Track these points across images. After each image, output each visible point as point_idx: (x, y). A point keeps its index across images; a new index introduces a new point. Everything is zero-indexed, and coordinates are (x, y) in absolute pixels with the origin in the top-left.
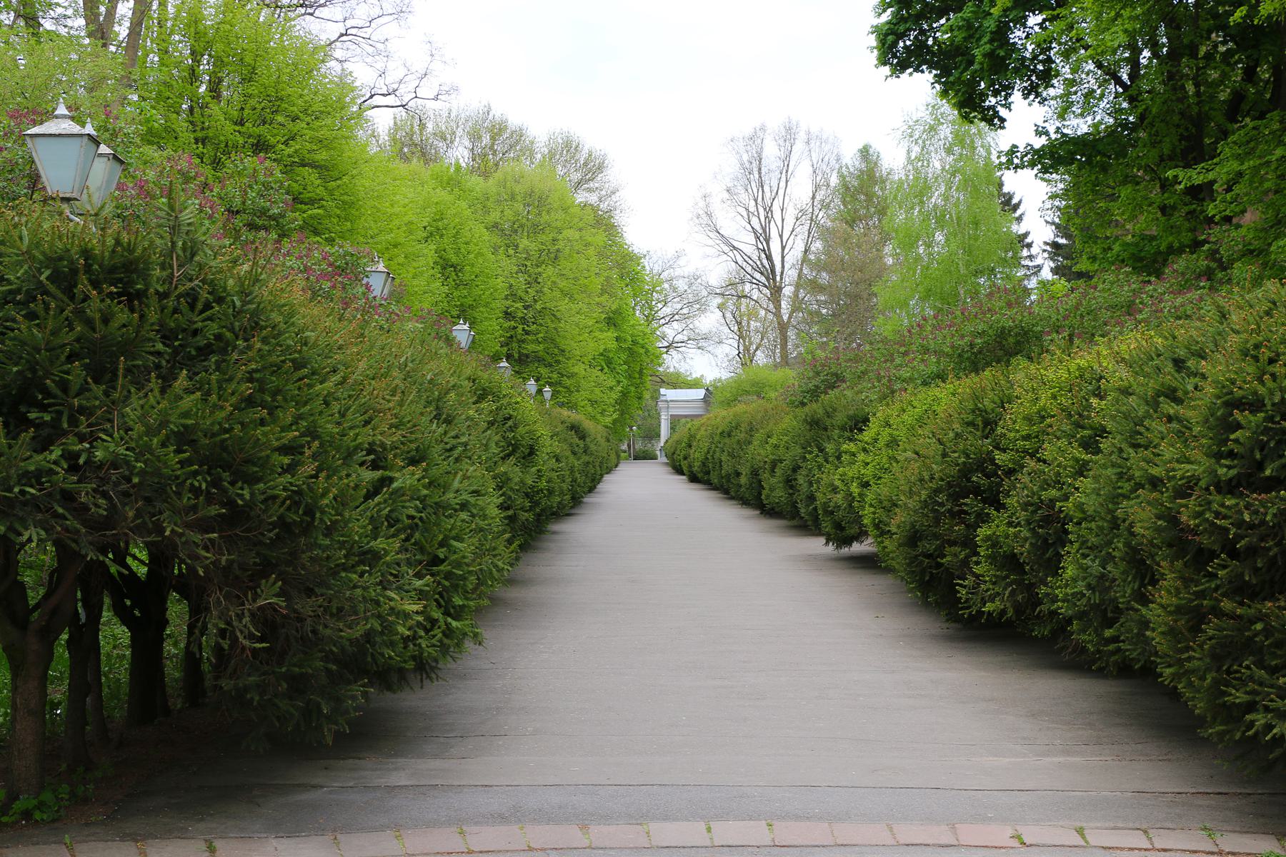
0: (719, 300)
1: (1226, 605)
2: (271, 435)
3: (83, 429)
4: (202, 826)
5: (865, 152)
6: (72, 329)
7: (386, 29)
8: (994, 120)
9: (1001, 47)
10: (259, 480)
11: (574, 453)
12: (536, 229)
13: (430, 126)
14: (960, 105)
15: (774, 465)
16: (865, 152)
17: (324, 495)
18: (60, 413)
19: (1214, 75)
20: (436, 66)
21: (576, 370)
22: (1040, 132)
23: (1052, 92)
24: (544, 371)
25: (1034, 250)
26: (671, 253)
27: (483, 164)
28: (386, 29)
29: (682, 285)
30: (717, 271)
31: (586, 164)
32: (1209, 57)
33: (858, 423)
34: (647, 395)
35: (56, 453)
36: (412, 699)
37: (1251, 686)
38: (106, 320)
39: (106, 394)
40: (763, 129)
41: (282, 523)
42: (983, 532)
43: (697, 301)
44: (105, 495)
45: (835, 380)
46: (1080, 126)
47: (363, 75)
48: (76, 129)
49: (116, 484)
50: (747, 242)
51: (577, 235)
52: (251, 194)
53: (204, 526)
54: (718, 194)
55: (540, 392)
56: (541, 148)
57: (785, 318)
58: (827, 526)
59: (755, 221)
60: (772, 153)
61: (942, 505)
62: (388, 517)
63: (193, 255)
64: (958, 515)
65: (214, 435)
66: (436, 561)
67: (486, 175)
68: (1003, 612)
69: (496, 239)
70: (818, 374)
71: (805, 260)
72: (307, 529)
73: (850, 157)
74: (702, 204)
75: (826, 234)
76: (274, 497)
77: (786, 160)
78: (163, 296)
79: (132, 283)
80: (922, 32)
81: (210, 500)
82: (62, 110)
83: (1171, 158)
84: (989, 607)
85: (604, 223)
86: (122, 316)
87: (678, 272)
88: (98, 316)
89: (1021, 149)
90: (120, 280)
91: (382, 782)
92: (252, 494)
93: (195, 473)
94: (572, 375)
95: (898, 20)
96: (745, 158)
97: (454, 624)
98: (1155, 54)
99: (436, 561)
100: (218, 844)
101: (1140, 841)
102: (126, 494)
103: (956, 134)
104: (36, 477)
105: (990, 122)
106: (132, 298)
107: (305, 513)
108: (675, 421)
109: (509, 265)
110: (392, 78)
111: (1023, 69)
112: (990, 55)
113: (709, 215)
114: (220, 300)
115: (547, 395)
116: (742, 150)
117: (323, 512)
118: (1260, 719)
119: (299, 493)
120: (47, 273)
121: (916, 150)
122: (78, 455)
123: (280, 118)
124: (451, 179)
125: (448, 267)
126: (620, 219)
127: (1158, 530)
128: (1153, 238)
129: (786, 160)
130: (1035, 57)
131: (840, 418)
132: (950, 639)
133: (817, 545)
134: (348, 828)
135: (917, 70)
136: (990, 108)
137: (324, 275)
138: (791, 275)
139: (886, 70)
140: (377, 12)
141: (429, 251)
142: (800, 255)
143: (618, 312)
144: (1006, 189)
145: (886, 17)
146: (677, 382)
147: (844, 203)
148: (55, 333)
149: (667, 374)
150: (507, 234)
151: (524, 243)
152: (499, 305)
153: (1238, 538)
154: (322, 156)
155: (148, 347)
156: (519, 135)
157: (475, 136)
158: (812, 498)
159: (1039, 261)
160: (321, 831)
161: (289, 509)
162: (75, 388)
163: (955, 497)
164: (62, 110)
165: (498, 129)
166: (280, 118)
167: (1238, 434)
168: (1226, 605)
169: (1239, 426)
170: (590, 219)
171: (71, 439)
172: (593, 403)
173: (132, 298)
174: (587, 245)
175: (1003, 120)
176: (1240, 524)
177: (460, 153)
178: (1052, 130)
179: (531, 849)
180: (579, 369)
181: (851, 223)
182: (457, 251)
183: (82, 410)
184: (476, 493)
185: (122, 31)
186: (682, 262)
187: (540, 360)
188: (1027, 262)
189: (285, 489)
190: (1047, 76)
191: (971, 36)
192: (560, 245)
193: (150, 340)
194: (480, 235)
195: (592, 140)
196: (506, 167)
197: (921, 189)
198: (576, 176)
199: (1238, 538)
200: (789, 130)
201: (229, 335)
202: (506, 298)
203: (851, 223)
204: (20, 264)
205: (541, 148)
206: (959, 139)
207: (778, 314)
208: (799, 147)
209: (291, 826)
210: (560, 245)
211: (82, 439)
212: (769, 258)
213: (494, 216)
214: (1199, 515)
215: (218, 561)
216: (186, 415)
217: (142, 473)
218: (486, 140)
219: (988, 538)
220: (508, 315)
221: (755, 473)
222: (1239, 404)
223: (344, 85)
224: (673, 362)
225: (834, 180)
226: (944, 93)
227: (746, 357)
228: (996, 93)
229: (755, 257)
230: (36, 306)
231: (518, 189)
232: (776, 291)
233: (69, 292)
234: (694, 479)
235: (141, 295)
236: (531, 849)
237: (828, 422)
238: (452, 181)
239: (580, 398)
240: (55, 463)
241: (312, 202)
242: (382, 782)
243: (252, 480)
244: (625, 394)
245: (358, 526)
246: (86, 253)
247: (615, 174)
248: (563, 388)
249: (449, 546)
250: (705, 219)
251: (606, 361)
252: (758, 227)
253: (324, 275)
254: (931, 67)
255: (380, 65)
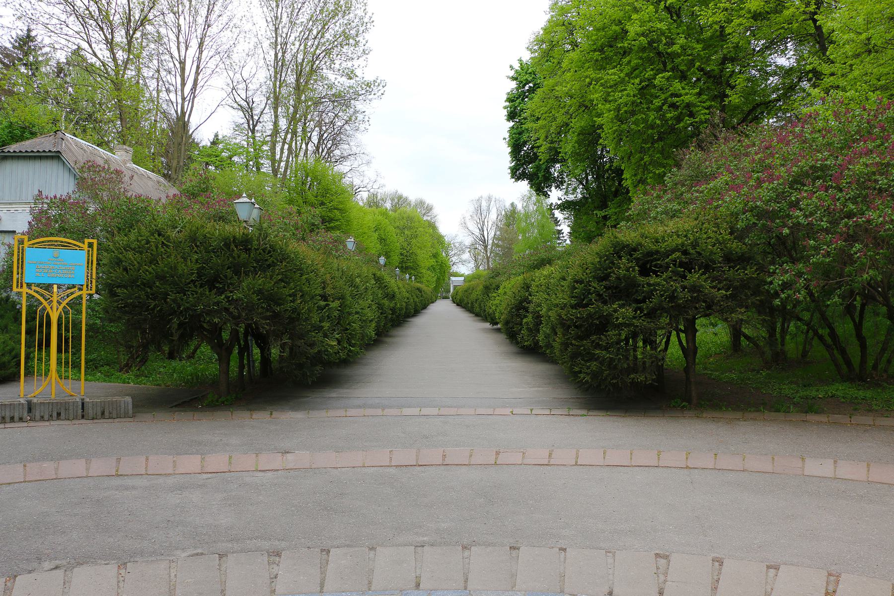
0: (469, 250)
1: (573, 342)
2: (286, 291)
3: (231, 289)
4: (271, 407)
5: (512, 204)
6: (228, 260)
7: (364, 168)
8: (547, 195)
9: (547, 173)
10: (283, 304)
11: (417, 297)
12: (410, 228)
13: (379, 198)
14: (536, 191)
15: (476, 300)
16: (512, 204)
17: (303, 309)
18: (225, 284)
19: (610, 183)
20: (379, 179)
21: (422, 271)
22: (559, 199)
23: (564, 187)
24: (412, 271)
25: (564, 235)
26: (454, 235)
27: (395, 208)
28: (364, 168)
29: (457, 245)
30: (468, 241)
31: (427, 207)
32: (608, 178)
33: (498, 287)
34: (447, 279)
35: (223, 296)
36: (347, 371)
37: (580, 366)
38: (239, 257)
39: (238, 279)
40: (482, 197)
41: (290, 317)
42: (525, 320)
43: (462, 250)
44: (238, 309)
45: (498, 275)
46: (571, 197)
47: (357, 182)
48: (248, 201)
49: (241, 306)
50: (477, 232)
51: (423, 230)
52: (309, 218)
53: (266, 318)
54: (468, 217)
55: (410, 278)
56: (413, 203)
57: (489, 255)
58: (489, 319)
59: (479, 225)
60: (484, 204)
61: (513, 312)
62: (328, 316)
63: (266, 237)
64: (518, 316)
65: (269, 291)
66: (347, 329)
67: (395, 211)
68: (531, 345)
69: (398, 231)
70: (493, 272)
71: (494, 237)
72: (298, 319)
73: (508, 205)
74: (463, 220)
75: (501, 229)
76: (288, 310)
77: (489, 207)
78: (256, 250)
79: (247, 246)
80: (524, 169)
81: (267, 310)
82: (244, 195)
83: (598, 208)
84: (526, 343)
85: (432, 226)
86: (244, 255)
87: (456, 241)
88: (236, 256)
89: (554, 204)
90: (244, 245)
91: (328, 396)
92: (280, 309)
93: (263, 302)
94: (421, 273)
95: (516, 165)
96: (476, 206)
97: (352, 349)
98: (593, 177)
99: (347, 329)
100: (273, 413)
101: (548, 412)
102: (243, 308)
103: (537, 199)
104: (217, 303)
105: (546, 196)
106: (247, 250)
107: (297, 314)
108: (455, 287)
109: (402, 239)
110: (365, 183)
111: (555, 180)
112: (544, 176)
113: (465, 223)
114: (274, 251)
115: (413, 279)
116: (475, 204)
117: (302, 314)
118: (582, 376)
119: (295, 308)
120: (223, 243)
121: (525, 204)
122: (229, 297)
123: (328, 195)
124: (384, 213)
125: (382, 240)
126: (437, 225)
127: (557, 319)
128: (593, 231)
129: (489, 207)
130: (558, 177)
131: (494, 286)
132: (518, 353)
133: (487, 325)
134: (313, 409)
135: (523, 180)
136: (545, 191)
137: (330, 243)
138: (490, 242)
139: (514, 180)
140: (360, 163)
141: (376, 235)
142: (493, 236)
143: (437, 253)
144: (555, 216)
145: (513, 164)
146: (456, 275)
147: (506, 220)
148: (223, 261)
149: (453, 272)
150: (402, 229)
151: (406, 232)
152: (398, 251)
153: (576, 322)
154: (341, 206)
155: (251, 265)
156: (406, 199)
157: (392, 200)
158: (485, 311)
159: (566, 238)
160: (305, 409)
161: (292, 313)
162: (229, 278)
163: (518, 310)
164: (244, 195)
165: (400, 197)
166: (328, 195)
167: (576, 291)
168: (573, 342)
169: (576, 288)
170: (427, 224)
171: (228, 292)
172: (428, 281)
173: (247, 250)
174: (427, 233)
175: (549, 195)
176: (577, 318)
177: (388, 205)
178: (563, 198)
179: (364, 416)
180: (424, 271)
181: (508, 226)
182: (385, 235)
183: (231, 284)
184: (362, 309)
185: (282, 170)
186: (457, 238)
187: (412, 268)
188: (562, 238)
189: (290, 307)
190: (562, 183)
191: (538, 170)
192: (418, 233)
193: (252, 263)
194: (391, 229)
195: (428, 201)
196: (402, 209)
197: (527, 215)
198: (423, 212)
199: (576, 322)
200: (489, 198)
201: (275, 261)
202: (401, 249)
203: (508, 226)
204: (215, 241)
205: (413, 203)
206: (538, 201)
207: (487, 255)
208: (493, 203)
209: (294, 409)
210: (418, 233)
211: (231, 292)
212: (484, 237)
213: (398, 224)
214: (566, 315)
215: (270, 329)
216: (260, 285)
217: (247, 303)
218: (396, 200)
219: (526, 323)
220: (402, 254)
221: (472, 303)
222: (577, 282)
223: (352, 185)
224: (454, 269)
225: (503, 213)
226: (531, 187)
227: (477, 267)
228: (547, 187)
229: (479, 236)
230: (219, 253)
231: (405, 216)
232: (486, 247)
233: (229, 248)
234: (458, 305)
235: (250, 249)
236: (364, 416)
237: (491, 287)
238: (385, 214)
239: (424, 280)
240: (223, 300)
241: (337, 220)
242: (328, 396)
243: (280, 305)
244: (438, 279)
245: (315, 318)
246: (234, 237)
247: (435, 211)
248: (418, 278)
249: (350, 325)
250: (464, 225)
251: (432, 268)
252: (480, 227)
253: (330, 243)
254: (527, 180)
255: (361, 179)
